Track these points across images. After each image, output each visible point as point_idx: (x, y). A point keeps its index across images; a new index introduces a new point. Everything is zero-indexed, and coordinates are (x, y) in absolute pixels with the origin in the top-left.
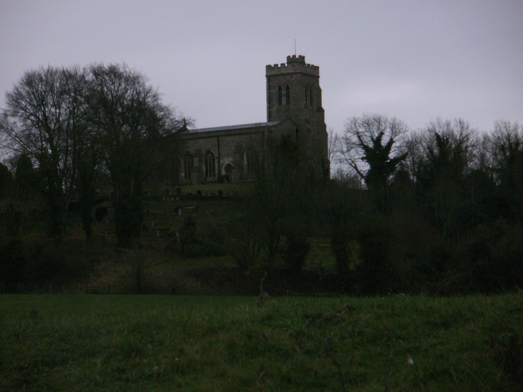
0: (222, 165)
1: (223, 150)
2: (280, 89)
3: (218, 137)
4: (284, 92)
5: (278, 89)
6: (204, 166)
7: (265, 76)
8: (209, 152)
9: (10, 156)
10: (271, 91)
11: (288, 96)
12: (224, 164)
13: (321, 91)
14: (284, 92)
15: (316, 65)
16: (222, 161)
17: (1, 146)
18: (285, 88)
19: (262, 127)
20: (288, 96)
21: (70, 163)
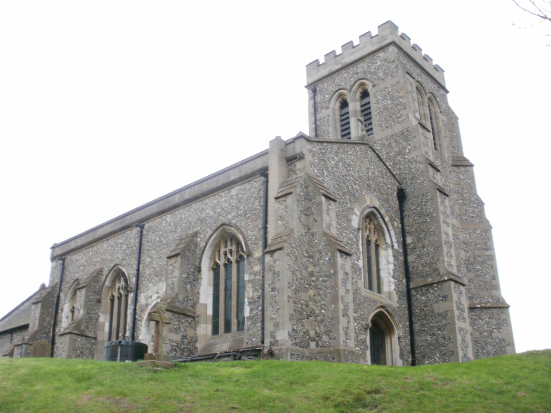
0: (143, 311)
1: (148, 260)
2: (344, 104)
3: (140, 224)
4: (354, 106)
5: (338, 104)
6: (104, 319)
7: (307, 87)
8: (119, 274)
9: (152, 345)
10: (318, 116)
11: (366, 112)
12: (147, 305)
13: (456, 118)
14: (354, 106)
15: (472, 161)
16: (142, 300)
17: (0, 344)
18: (358, 95)
19: (406, 249)
20: (366, 112)
21: (435, 330)
